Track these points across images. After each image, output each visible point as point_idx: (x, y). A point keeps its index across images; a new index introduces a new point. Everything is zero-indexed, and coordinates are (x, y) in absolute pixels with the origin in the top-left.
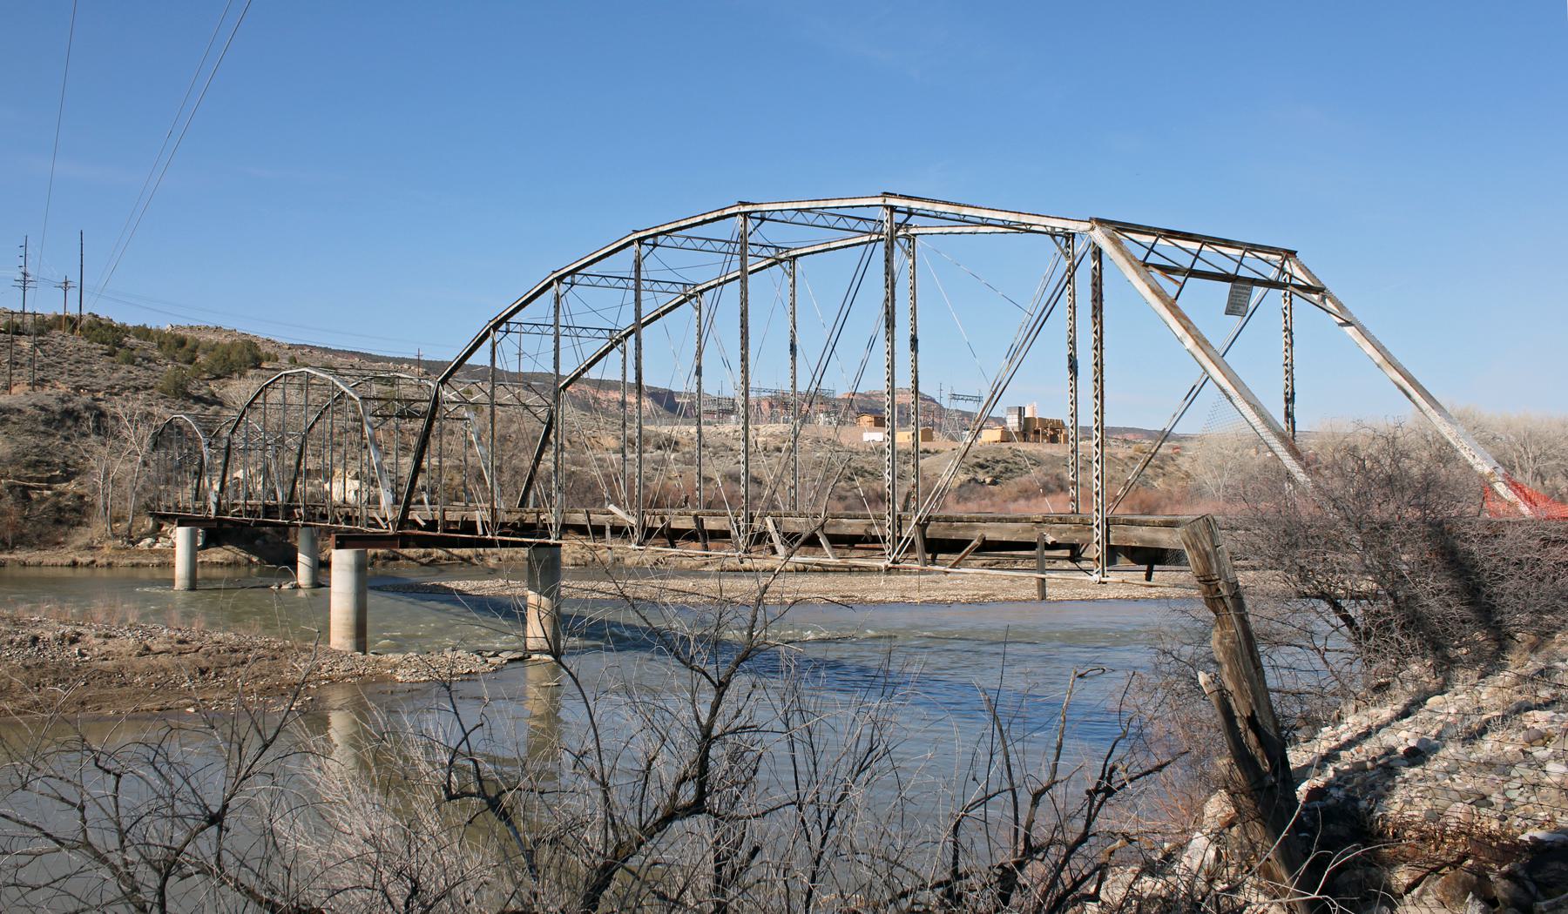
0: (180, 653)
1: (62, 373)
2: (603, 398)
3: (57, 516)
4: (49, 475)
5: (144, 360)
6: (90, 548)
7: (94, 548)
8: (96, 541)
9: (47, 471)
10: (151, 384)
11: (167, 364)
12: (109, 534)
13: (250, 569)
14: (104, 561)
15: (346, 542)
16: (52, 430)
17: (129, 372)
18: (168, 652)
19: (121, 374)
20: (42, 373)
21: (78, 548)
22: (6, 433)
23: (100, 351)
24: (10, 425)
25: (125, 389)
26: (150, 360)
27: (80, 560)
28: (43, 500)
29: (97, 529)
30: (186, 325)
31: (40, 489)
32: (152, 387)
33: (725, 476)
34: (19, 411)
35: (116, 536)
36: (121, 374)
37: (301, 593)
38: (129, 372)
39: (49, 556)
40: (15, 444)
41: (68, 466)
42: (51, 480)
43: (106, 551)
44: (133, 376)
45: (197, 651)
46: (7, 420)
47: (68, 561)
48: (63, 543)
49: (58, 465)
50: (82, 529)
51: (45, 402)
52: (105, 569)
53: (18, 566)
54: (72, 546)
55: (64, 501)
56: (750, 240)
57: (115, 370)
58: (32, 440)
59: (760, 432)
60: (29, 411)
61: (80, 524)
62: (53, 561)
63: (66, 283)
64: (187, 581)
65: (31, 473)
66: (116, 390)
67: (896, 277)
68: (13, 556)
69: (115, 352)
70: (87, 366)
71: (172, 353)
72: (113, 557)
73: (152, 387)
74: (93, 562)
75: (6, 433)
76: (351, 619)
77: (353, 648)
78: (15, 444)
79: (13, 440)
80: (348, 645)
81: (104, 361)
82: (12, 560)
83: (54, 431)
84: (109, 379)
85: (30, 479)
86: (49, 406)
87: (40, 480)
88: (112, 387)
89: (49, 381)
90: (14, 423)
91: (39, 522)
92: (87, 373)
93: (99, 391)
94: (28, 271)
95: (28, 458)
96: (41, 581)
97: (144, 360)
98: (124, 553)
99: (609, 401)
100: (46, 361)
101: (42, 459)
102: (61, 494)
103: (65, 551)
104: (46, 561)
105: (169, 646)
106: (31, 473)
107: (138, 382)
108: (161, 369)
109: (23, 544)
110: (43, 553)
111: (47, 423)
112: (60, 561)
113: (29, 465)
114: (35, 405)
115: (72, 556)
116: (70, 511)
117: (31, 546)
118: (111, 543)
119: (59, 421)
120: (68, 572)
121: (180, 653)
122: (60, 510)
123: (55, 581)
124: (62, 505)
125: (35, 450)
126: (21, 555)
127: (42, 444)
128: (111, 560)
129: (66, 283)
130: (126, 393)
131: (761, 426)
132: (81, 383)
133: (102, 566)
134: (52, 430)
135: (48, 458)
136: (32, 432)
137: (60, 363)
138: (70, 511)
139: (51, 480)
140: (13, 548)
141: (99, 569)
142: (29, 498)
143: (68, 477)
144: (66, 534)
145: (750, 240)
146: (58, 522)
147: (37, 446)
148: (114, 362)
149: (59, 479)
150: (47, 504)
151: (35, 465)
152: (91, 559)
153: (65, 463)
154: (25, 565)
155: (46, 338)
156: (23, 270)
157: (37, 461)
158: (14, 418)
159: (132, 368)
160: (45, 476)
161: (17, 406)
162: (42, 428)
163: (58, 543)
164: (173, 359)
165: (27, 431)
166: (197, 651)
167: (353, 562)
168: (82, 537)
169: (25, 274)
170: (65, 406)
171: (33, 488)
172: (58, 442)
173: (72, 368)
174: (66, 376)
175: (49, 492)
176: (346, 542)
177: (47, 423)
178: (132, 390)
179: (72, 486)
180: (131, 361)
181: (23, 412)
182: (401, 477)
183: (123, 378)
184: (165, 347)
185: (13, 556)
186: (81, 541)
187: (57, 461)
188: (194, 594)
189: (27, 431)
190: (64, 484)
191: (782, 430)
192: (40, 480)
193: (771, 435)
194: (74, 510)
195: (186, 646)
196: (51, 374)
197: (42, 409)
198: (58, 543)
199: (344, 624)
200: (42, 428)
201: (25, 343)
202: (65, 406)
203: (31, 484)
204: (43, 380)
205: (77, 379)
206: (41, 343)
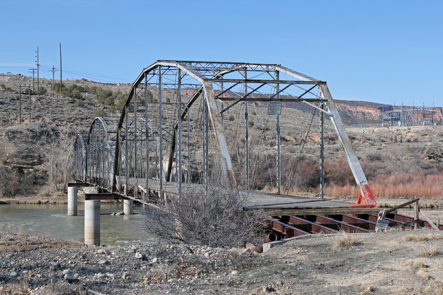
0: (9, 245)
1: (48, 113)
2: (354, 111)
3: (34, 181)
4: (32, 162)
5: (88, 105)
6: (48, 195)
7: (50, 195)
8: (50, 192)
9: (31, 160)
10: (89, 116)
11: (99, 106)
12: (56, 189)
13: (118, 205)
14: (52, 201)
15: (91, 197)
16: (35, 141)
17: (80, 111)
18: (4, 244)
19: (76, 112)
20: (39, 113)
21: (42, 196)
22: (14, 143)
23: (68, 101)
24: (16, 139)
25: (76, 119)
26: (91, 104)
27: (42, 201)
28: (30, 173)
29: (50, 187)
30: (126, 83)
31: (28, 168)
32: (89, 118)
33: (368, 156)
34: (21, 132)
35: (58, 190)
36: (76, 112)
37: (125, 217)
38: (80, 111)
39: (30, 199)
40: (18, 148)
41: (41, 157)
42: (33, 164)
43: (54, 197)
44: (81, 113)
45: (17, 244)
46: (15, 137)
47: (37, 201)
48: (36, 193)
49: (36, 157)
50: (45, 187)
51: (33, 128)
52: (53, 205)
53: (15, 204)
54: (40, 194)
55: (38, 174)
56: (148, 83)
57: (73, 110)
58: (25, 146)
59: (411, 130)
60: (26, 132)
61: (43, 184)
62: (30, 201)
63: (54, 69)
64: (73, 212)
65: (24, 161)
66: (72, 120)
67: (271, 84)
68: (14, 199)
69: (75, 101)
70: (60, 109)
71: (102, 100)
72: (57, 200)
73: (89, 118)
74: (48, 202)
75: (14, 143)
76: (92, 231)
77: (93, 243)
78: (18, 148)
79: (17, 146)
80: (90, 242)
81: (69, 106)
82: (14, 201)
83: (36, 141)
84: (70, 115)
85: (24, 164)
86: (35, 129)
87: (28, 164)
88: (70, 119)
89: (42, 117)
90: (18, 138)
91: (26, 183)
92: (60, 112)
93: (64, 121)
94: (40, 63)
95: (23, 154)
96: (26, 210)
97: (88, 105)
98: (62, 197)
99: (357, 112)
100: (42, 107)
101: (29, 154)
102: (37, 170)
103: (36, 197)
104: (28, 201)
105: (5, 242)
106: (24, 161)
107: (83, 116)
108: (96, 108)
109: (19, 193)
110: (27, 198)
111: (33, 138)
112: (33, 201)
113: (23, 158)
114: (28, 129)
115: (39, 199)
116: (40, 178)
117: (22, 194)
118: (57, 193)
119: (38, 136)
120: (37, 207)
121: (9, 245)
122: (36, 178)
123: (32, 210)
124: (37, 176)
125: (26, 150)
126: (17, 199)
127: (29, 148)
128: (55, 201)
129: (54, 69)
130: (77, 121)
131: (411, 127)
132: (56, 117)
133: (52, 204)
134: (35, 141)
135: (31, 154)
136: (26, 142)
137: (48, 108)
138: (40, 178)
139: (33, 164)
140: (14, 195)
141: (50, 205)
142: (23, 173)
143: (40, 162)
144: (37, 189)
145: (148, 83)
146: (35, 183)
147: (27, 148)
148: (73, 106)
149: (36, 163)
150: (31, 175)
151: (26, 157)
152: (47, 200)
153: (39, 156)
154: (18, 203)
155: (43, 96)
156: (37, 63)
157: (27, 156)
158: (18, 136)
159: (81, 109)
160: (30, 162)
161: (20, 130)
162: (30, 140)
163: (34, 193)
164: (103, 103)
165: (23, 142)
166: (17, 244)
167: (92, 206)
168: (44, 190)
169: (38, 65)
170: (42, 129)
171: (25, 168)
172: (37, 146)
173: (54, 110)
174: (49, 114)
175: (32, 170)
176: (91, 197)
177: (33, 138)
178: (79, 120)
179: (41, 167)
180: (82, 105)
181: (23, 133)
182: (195, 160)
183: (76, 114)
184: (100, 97)
185: (14, 199)
186: (44, 192)
187: (36, 155)
188: (75, 217)
189: (23, 142)
190: (39, 166)
191: (422, 129)
192: (28, 164)
193: (417, 132)
194: (42, 178)
195: (13, 242)
196: (43, 113)
197: (31, 131)
198: (34, 193)
199: (89, 233)
200: (30, 140)
201: (34, 99)
202: (42, 129)
203: (24, 166)
204: (39, 116)
205: (55, 115)
206: (41, 98)
